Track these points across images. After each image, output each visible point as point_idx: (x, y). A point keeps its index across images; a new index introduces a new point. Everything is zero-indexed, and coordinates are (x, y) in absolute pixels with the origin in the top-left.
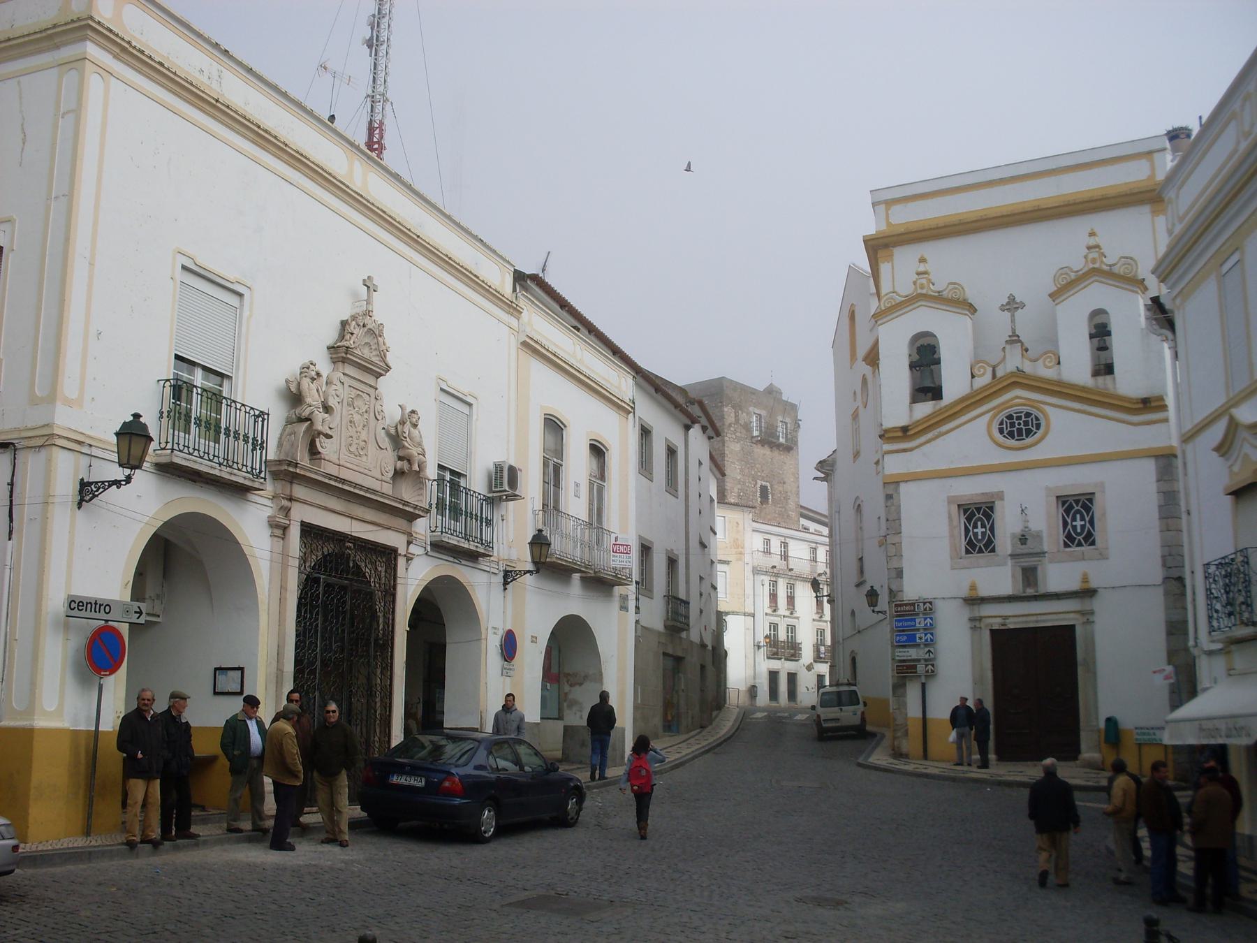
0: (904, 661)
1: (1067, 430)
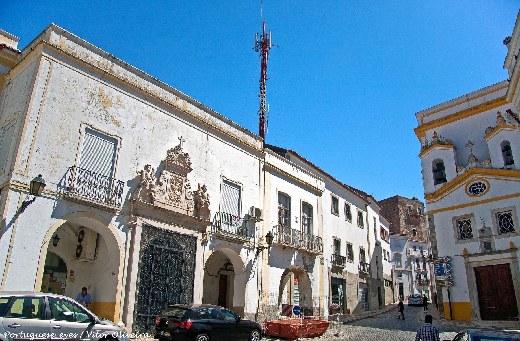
0: (440, 281)
1: (496, 185)
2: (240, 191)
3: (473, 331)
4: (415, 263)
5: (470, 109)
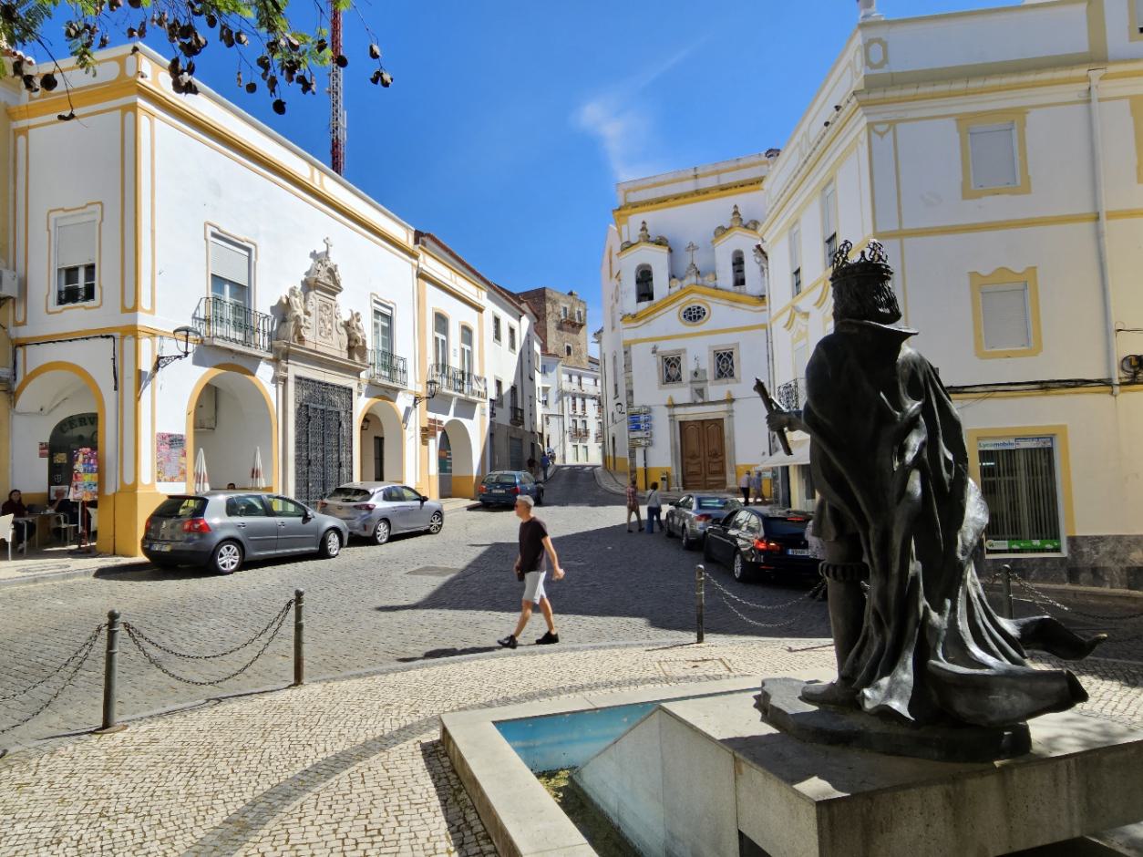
2: (249, 258)
3: (173, 543)
4: (570, 399)
5: (697, 192)
